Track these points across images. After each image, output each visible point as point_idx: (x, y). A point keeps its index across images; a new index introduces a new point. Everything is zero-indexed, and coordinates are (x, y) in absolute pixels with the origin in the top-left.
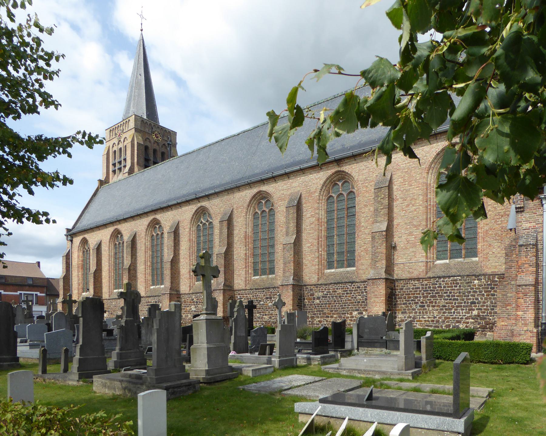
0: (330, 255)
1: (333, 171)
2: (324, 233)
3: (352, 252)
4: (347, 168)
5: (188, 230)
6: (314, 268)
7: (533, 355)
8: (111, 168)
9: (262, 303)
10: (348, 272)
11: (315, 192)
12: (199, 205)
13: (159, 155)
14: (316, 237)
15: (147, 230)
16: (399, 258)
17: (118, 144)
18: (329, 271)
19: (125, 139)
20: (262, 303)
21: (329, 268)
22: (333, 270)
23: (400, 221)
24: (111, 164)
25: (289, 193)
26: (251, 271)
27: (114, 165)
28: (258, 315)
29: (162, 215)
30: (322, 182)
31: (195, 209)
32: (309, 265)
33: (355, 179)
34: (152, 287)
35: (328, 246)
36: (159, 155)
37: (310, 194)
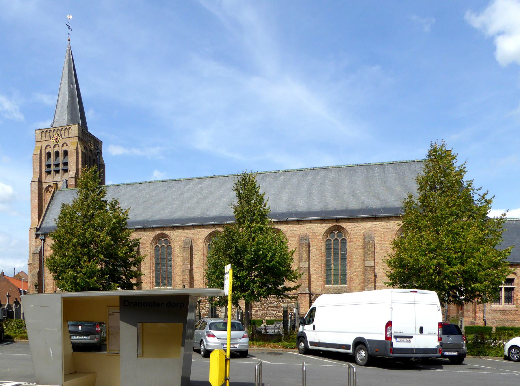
0: (328, 276)
1: (333, 224)
2: (324, 262)
3: (344, 275)
4: (343, 225)
5: (201, 247)
6: (319, 283)
7: (450, 229)
8: (44, 168)
9: (276, 304)
10: (342, 287)
11: (319, 236)
12: (214, 229)
13: (92, 161)
14: (320, 264)
15: (152, 241)
16: (313, 285)
17: (54, 147)
18: (327, 286)
19: (63, 144)
20: (276, 304)
21: (327, 284)
22: (330, 286)
23: (379, 261)
24: (44, 165)
25: (298, 233)
26: (154, 284)
27: (49, 166)
28: (272, 312)
29: (171, 232)
30: (325, 230)
31: (210, 232)
32: (315, 281)
33: (349, 232)
34: (155, 288)
35: (327, 270)
36: (92, 161)
37: (316, 236)
